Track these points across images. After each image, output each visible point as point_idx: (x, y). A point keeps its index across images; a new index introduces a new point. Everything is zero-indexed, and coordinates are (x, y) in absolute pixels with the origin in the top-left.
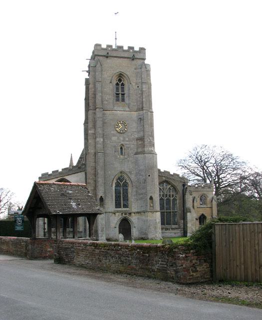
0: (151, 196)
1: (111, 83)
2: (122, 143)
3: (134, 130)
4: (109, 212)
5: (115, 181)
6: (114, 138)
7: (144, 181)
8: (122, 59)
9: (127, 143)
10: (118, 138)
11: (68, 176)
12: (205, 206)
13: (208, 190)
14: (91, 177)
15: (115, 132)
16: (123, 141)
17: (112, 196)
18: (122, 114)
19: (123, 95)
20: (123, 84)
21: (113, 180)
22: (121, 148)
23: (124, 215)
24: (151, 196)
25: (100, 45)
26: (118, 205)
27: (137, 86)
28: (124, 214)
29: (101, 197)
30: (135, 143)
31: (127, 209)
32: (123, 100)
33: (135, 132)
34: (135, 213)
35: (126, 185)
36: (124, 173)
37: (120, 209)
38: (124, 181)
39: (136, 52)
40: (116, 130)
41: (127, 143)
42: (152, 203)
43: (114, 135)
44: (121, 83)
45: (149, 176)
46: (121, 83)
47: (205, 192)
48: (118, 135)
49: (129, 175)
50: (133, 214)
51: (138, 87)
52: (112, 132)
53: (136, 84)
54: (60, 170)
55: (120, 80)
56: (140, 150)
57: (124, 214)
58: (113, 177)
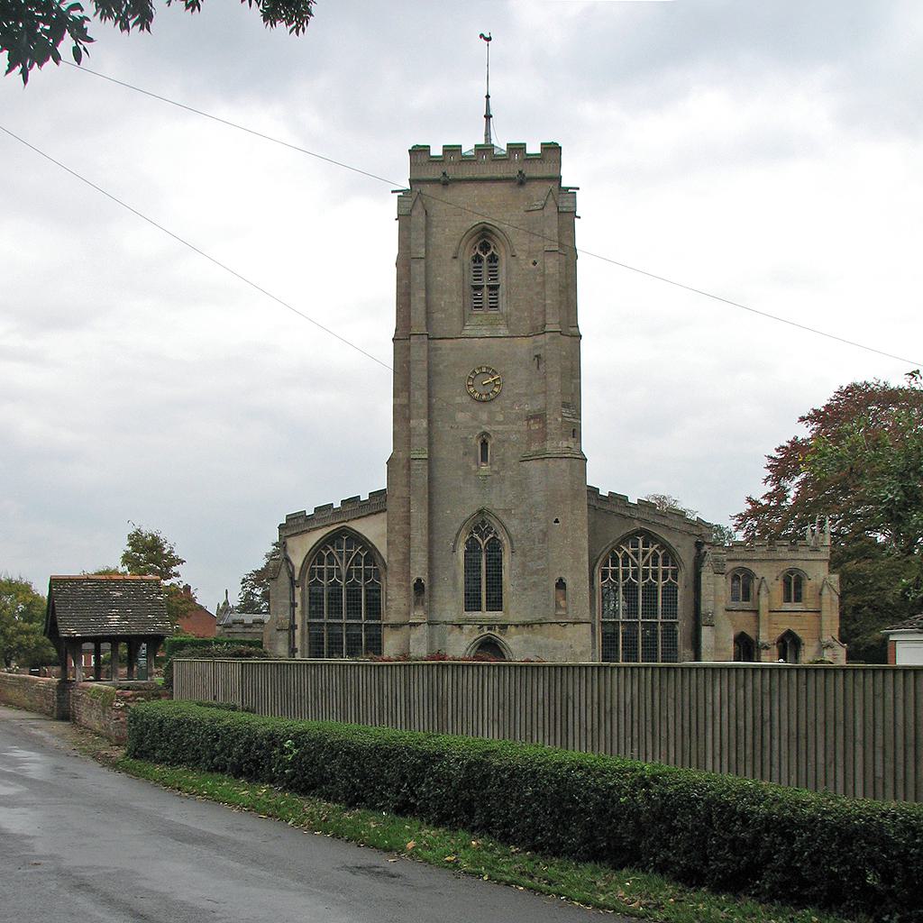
0: (561, 580)
1: (455, 258)
2: (487, 428)
3: (522, 391)
4: (445, 623)
5: (464, 537)
6: (460, 416)
7: (541, 537)
8: (488, 184)
9: (500, 428)
10: (474, 418)
11: (363, 521)
12: (798, 607)
13: (811, 556)
14: (397, 527)
15: (466, 399)
16: (489, 423)
17: (455, 578)
18: (488, 347)
19: (494, 288)
20: (493, 259)
21: (457, 535)
22: (484, 444)
23: (486, 632)
24: (561, 580)
25: (426, 149)
26: (472, 602)
27: (531, 261)
28: (485, 628)
29: (419, 580)
30: (525, 428)
31: (499, 614)
32: (494, 305)
33: (526, 395)
34: (517, 626)
35: (495, 547)
36: (489, 513)
37: (477, 614)
38: (491, 536)
39: (532, 159)
40: (470, 394)
41: (500, 428)
42: (565, 599)
43: (463, 408)
44: (489, 254)
45: (557, 521)
46: (489, 254)
47: (799, 565)
48: (476, 406)
49: (504, 519)
50: (512, 629)
51: (535, 263)
52: (458, 400)
53: (530, 254)
54: (364, 497)
55: (485, 247)
56: (535, 447)
57: (485, 628)
58: (458, 525)
